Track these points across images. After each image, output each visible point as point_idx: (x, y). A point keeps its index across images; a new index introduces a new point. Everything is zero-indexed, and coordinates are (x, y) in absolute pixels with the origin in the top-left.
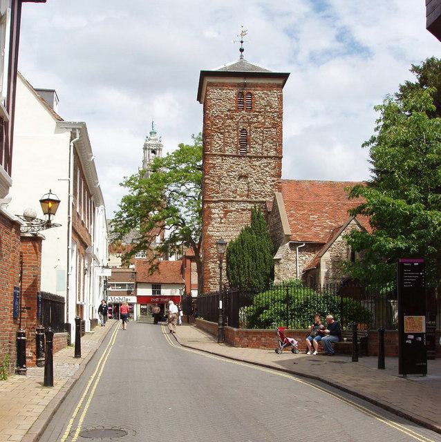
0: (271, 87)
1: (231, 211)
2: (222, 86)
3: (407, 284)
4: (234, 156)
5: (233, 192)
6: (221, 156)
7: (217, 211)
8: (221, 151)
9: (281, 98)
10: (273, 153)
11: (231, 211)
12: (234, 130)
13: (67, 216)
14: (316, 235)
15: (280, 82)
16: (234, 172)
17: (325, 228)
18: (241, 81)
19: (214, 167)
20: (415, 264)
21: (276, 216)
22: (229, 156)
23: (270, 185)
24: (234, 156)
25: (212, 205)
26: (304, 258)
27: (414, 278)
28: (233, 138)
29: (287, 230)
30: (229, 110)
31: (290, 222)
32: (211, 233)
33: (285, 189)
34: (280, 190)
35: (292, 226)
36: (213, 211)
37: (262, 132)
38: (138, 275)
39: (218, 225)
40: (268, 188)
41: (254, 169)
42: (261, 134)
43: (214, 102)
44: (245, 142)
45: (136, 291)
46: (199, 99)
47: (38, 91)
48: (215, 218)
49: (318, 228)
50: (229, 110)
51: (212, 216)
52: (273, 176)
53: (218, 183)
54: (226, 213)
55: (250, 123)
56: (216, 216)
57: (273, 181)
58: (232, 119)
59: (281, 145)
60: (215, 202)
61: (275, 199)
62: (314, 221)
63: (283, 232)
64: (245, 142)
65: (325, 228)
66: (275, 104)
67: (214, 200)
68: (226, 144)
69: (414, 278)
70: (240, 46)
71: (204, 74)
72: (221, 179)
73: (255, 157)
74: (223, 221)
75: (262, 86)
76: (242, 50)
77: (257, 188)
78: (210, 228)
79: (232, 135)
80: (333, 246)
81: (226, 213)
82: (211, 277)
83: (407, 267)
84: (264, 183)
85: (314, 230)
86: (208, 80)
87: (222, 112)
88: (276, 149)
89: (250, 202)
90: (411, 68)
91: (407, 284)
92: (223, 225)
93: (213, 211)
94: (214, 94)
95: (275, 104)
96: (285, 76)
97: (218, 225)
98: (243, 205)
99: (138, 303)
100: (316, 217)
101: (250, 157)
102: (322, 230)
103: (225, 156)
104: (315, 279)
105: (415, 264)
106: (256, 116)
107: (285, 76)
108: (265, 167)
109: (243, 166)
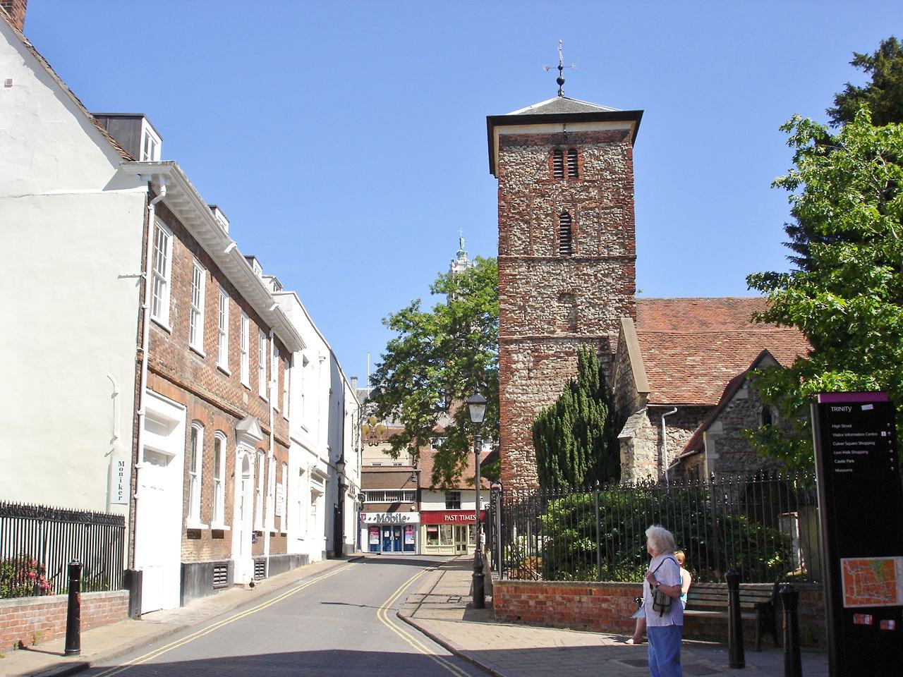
0: (612, 139)
1: (547, 357)
2: (525, 142)
3: (842, 466)
4: (549, 260)
5: (549, 323)
6: (526, 260)
7: (521, 357)
8: (525, 253)
9: (628, 157)
10: (617, 252)
11: (547, 357)
12: (547, 215)
13: (134, 348)
14: (698, 391)
15: (627, 126)
16: (551, 287)
17: (716, 378)
18: (557, 129)
19: (514, 279)
20: (864, 408)
21: (624, 361)
22: (540, 260)
23: (616, 308)
24: (549, 260)
25: (513, 346)
26: (676, 435)
27: (863, 448)
28: (547, 230)
29: (642, 382)
30: (538, 182)
31: (648, 370)
32: (514, 397)
33: (644, 313)
34: (633, 314)
35: (652, 376)
36: (515, 357)
37: (598, 217)
38: (421, 475)
39: (524, 382)
40: (611, 313)
41: (586, 282)
42: (595, 220)
43: (511, 169)
44: (567, 235)
45: (419, 507)
46: (492, 171)
47: (101, 119)
48: (517, 370)
49: (703, 380)
50: (538, 182)
51: (514, 366)
52: (621, 292)
53: (522, 308)
54: (538, 360)
55: (574, 201)
56: (520, 365)
57: (621, 300)
58: (543, 196)
59: (633, 236)
60: (517, 342)
61: (621, 333)
62: (693, 366)
63: (635, 387)
64: (567, 235)
65: (716, 378)
66: (619, 166)
67: (515, 337)
68: (533, 240)
69: (863, 448)
70: (556, 74)
71: (489, 118)
72: (528, 301)
73: (587, 260)
74: (532, 374)
75: (596, 139)
76: (560, 82)
77: (590, 314)
78: (510, 388)
79: (544, 224)
80: (728, 410)
81: (538, 360)
82: (514, 476)
83: (841, 417)
84: (605, 305)
85: (694, 382)
86: (499, 131)
87: (527, 186)
88: (623, 245)
89: (581, 340)
90: (852, 58)
91: (842, 466)
92: (533, 381)
93: (515, 357)
94: (509, 158)
95: (619, 166)
96: (636, 116)
97: (524, 382)
98: (568, 346)
99: (422, 524)
100: (698, 359)
101: (579, 261)
102: (709, 383)
103: (533, 260)
104: (697, 473)
105: (864, 408)
106: (586, 189)
107: (636, 116)
108: (604, 275)
109: (565, 277)
